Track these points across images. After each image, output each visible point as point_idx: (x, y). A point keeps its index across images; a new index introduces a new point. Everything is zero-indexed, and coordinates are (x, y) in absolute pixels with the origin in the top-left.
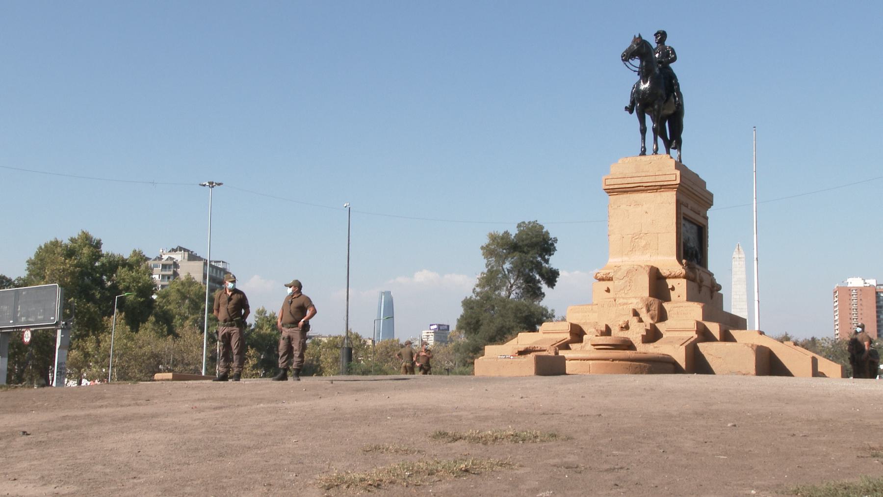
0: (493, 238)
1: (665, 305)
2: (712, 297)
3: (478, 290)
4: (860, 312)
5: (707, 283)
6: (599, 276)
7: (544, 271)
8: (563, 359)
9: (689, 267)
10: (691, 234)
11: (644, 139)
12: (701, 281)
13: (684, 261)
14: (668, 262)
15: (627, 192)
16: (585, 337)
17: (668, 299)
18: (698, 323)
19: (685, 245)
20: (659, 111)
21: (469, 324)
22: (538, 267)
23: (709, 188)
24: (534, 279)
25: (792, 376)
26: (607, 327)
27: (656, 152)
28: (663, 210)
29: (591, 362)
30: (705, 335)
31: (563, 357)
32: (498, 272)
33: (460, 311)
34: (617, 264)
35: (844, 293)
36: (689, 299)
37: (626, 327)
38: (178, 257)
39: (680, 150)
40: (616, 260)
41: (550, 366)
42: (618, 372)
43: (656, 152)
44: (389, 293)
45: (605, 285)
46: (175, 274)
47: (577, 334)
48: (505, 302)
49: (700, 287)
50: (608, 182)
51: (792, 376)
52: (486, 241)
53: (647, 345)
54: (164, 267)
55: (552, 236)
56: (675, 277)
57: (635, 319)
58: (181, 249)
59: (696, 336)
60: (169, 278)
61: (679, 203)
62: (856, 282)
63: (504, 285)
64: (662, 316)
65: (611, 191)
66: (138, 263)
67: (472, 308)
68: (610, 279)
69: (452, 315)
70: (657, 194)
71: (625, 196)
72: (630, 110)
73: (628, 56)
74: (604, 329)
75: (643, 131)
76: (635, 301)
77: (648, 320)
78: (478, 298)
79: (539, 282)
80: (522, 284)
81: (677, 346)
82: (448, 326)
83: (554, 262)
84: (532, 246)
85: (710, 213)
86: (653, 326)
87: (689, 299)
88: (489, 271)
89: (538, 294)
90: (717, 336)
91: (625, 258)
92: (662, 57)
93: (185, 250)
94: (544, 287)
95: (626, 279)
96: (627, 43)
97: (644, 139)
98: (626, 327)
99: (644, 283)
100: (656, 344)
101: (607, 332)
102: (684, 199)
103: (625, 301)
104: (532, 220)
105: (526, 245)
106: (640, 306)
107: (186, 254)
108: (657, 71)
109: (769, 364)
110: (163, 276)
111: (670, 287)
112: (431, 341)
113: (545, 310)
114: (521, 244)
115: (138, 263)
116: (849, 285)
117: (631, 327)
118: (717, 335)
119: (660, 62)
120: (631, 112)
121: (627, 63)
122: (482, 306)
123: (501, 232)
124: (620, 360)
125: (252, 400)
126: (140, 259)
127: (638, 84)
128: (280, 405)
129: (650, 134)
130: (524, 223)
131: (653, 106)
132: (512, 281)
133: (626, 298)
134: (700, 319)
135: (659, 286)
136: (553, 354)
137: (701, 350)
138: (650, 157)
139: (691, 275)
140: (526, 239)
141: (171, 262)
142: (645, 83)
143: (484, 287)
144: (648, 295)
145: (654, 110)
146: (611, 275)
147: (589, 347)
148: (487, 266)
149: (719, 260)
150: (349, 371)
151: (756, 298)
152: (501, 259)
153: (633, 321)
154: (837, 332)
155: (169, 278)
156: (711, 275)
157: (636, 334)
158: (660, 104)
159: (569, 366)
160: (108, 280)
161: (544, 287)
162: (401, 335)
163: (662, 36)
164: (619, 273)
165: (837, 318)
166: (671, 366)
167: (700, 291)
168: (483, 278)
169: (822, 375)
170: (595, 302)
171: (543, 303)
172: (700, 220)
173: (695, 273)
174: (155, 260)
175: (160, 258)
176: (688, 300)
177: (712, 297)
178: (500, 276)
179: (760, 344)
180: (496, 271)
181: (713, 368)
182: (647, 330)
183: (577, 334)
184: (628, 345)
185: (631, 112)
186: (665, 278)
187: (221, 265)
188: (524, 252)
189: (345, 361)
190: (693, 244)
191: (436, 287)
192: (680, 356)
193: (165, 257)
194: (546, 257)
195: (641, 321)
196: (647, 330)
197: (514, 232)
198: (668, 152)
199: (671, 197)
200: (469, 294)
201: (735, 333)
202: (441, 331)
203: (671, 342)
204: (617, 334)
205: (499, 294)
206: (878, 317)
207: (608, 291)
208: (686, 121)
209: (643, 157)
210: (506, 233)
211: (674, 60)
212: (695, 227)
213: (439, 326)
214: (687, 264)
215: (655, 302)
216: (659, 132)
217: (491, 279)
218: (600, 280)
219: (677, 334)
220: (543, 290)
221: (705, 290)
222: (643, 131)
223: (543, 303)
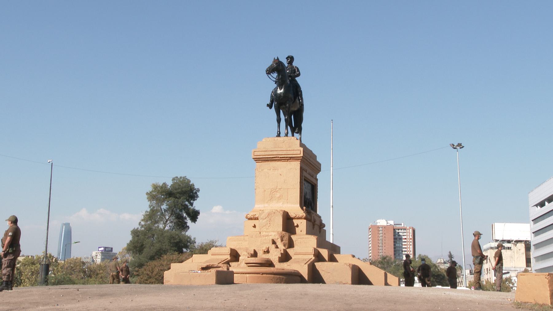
0: (155, 187)
1: (292, 237)
2: (320, 232)
3: (143, 223)
4: (384, 242)
5: (317, 222)
6: (249, 216)
7: (191, 211)
8: (232, 273)
9: (307, 212)
10: (308, 190)
11: (279, 126)
12: (315, 221)
13: (304, 208)
14: (295, 209)
15: (268, 161)
16: (240, 258)
17: (294, 233)
18: (315, 249)
19: (305, 197)
20: (289, 108)
21: (135, 247)
22: (186, 208)
23: (318, 159)
24: (182, 217)
26: (255, 251)
27: (287, 135)
28: (292, 172)
29: (248, 275)
30: (319, 258)
31: (233, 272)
32: (157, 211)
34: (263, 209)
35: (375, 229)
36: (308, 233)
37: (268, 252)
39: (301, 134)
40: (259, 206)
42: (266, 282)
43: (287, 135)
44: (69, 224)
45: (253, 222)
47: (234, 256)
48: (162, 231)
50: (256, 153)
52: (150, 189)
53: (282, 264)
55: (196, 187)
57: (274, 246)
59: (314, 258)
62: (382, 222)
63: (161, 221)
64: (291, 244)
65: (257, 160)
67: (138, 236)
68: (257, 219)
70: (288, 163)
71: (267, 163)
72: (270, 106)
73: (270, 71)
74: (253, 252)
75: (279, 121)
76: (273, 234)
77: (281, 247)
78: (143, 229)
79: (186, 218)
80: (174, 219)
81: (303, 264)
82: (112, 248)
83: (197, 205)
84: (183, 193)
85: (319, 176)
87: (308, 233)
88: (151, 210)
89: (183, 226)
90: (327, 258)
91: (266, 205)
92: (291, 73)
94: (189, 222)
95: (267, 219)
96: (269, 63)
97: (279, 126)
98: (268, 252)
100: (288, 263)
101: (255, 254)
102: (305, 167)
103: (267, 234)
104: (183, 176)
105: (178, 193)
106: (276, 237)
108: (288, 82)
109: (359, 278)
111: (295, 225)
112: (98, 260)
113: (189, 238)
114: (175, 191)
116: (378, 224)
117: (271, 251)
118: (326, 258)
119: (290, 76)
120: (271, 107)
121: (269, 75)
122: (145, 235)
123: (161, 184)
124: (267, 274)
125: (30, 303)
127: (276, 90)
130: (177, 177)
131: (285, 105)
133: (267, 232)
134: (315, 247)
136: (225, 269)
137: (317, 267)
138: (282, 138)
139: (309, 217)
140: (179, 189)
142: (281, 89)
143: (147, 221)
145: (286, 107)
146: (257, 216)
148: (150, 206)
149: (325, 208)
150: (46, 282)
151: (331, 232)
152: (160, 201)
154: (370, 255)
156: (320, 217)
157: (274, 256)
158: (289, 104)
159: (236, 278)
161: (189, 222)
162: (77, 253)
163: (291, 59)
164: (263, 215)
165: (370, 245)
166: (299, 278)
167: (313, 228)
168: (146, 215)
170: (246, 234)
171: (188, 233)
173: (311, 216)
177: (320, 232)
178: (159, 213)
179: (354, 264)
181: (325, 279)
182: (282, 254)
183: (235, 256)
184: (270, 264)
185: (271, 107)
186: (292, 219)
188: (176, 198)
189: (43, 274)
190: (309, 196)
191: (108, 221)
192: (304, 272)
195: (277, 247)
196: (282, 254)
197: (169, 183)
198: (293, 135)
199: (296, 166)
200: (136, 226)
201: (336, 256)
203: (298, 262)
204: (262, 256)
205: (158, 226)
206: (394, 245)
207: (255, 226)
208: (305, 115)
209: (279, 138)
210: (164, 184)
211: (299, 75)
212: (310, 185)
213: (105, 248)
214: (306, 210)
215: (287, 235)
218: (249, 219)
220: (188, 224)
221: (316, 227)
222: (279, 121)
223: (188, 233)
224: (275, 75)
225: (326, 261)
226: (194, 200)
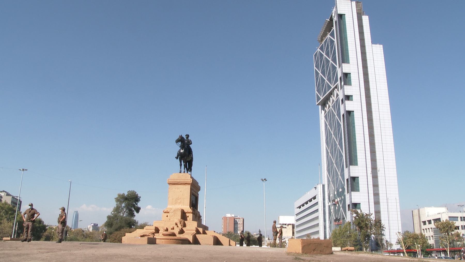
3: (113, 213)
5: (198, 215)
8: (156, 239)
9: (193, 210)
10: (194, 200)
11: (181, 168)
14: (187, 208)
21: (109, 224)
22: (134, 206)
25: (200, 244)
27: (184, 172)
28: (187, 190)
30: (198, 232)
32: (120, 207)
33: (106, 220)
35: (225, 218)
41: (152, 241)
43: (184, 172)
45: (166, 214)
48: (122, 217)
49: (196, 216)
51: (200, 244)
52: (117, 196)
55: (139, 196)
56: (189, 213)
58: (4, 191)
61: (191, 189)
62: (229, 215)
64: (185, 225)
68: (168, 213)
69: (102, 221)
72: (177, 158)
73: (177, 141)
76: (176, 220)
77: (180, 227)
83: (139, 204)
84: (132, 199)
85: (199, 193)
86: (182, 228)
89: (133, 215)
94: (135, 213)
96: (177, 137)
97: (181, 168)
98: (173, 229)
99: (179, 214)
100: (183, 234)
101: (167, 230)
102: (192, 188)
109: (217, 242)
112: (91, 230)
113: (135, 221)
127: (180, 150)
129: (183, 166)
135: (184, 216)
147: (161, 235)
149: (201, 208)
152: (121, 203)
157: (176, 231)
158: (186, 157)
163: (188, 136)
169: (221, 244)
171: (135, 218)
172: (197, 195)
176: (193, 220)
183: (157, 230)
184: (174, 235)
190: (194, 202)
191: (94, 211)
192: (191, 239)
195: (178, 227)
197: (126, 194)
199: (189, 187)
200: (110, 214)
201: (206, 231)
202: (95, 227)
203: (188, 234)
204: (170, 231)
207: (167, 216)
211: (191, 144)
215: (183, 221)
216: (185, 166)
217: (117, 209)
219: (189, 231)
221: (197, 217)
222: (181, 165)
223: (135, 218)
224: (180, 143)
225: (201, 234)
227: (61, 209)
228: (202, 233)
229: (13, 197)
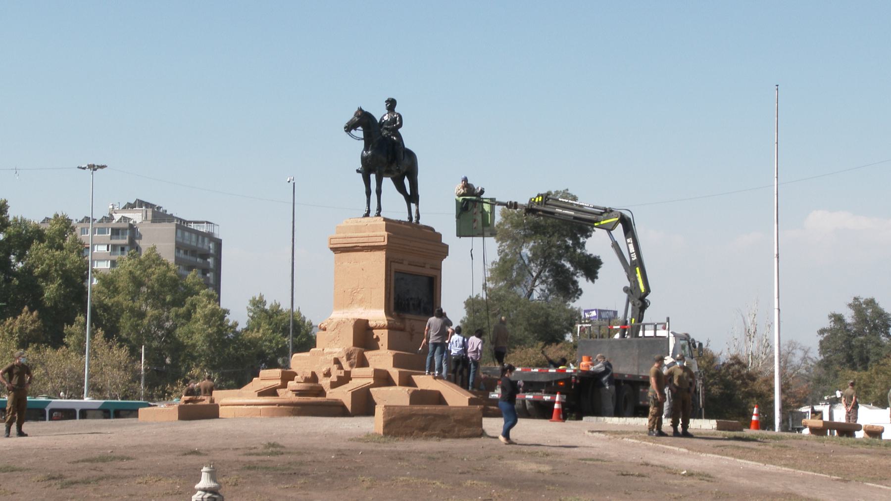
3: (490, 285)
26: (313, 374)
38: (136, 217)
46: (133, 244)
50: (333, 241)
54: (116, 232)
56: (380, 328)
58: (141, 203)
60: (123, 249)
66: (62, 234)
73: (350, 127)
74: (309, 375)
93: (148, 205)
94: (582, 281)
95: (336, 331)
96: (349, 115)
107: (150, 213)
110: (114, 247)
111: (375, 337)
115: (62, 234)
126: (65, 225)
128: (840, 456)
132: (534, 274)
141: (126, 225)
144: (352, 344)
148: (500, 252)
153: (334, 368)
155: (123, 249)
159: (222, 411)
160: (18, 260)
161: (582, 281)
168: (496, 269)
174: (101, 221)
175: (111, 218)
180: (510, 260)
187: (203, 229)
193: (117, 217)
194: (582, 240)
209: (367, 218)
213: (600, 312)
224: (359, 133)
225: (395, 385)
226: (587, 237)
227: (261, 297)
228: (397, 383)
229: (182, 226)
